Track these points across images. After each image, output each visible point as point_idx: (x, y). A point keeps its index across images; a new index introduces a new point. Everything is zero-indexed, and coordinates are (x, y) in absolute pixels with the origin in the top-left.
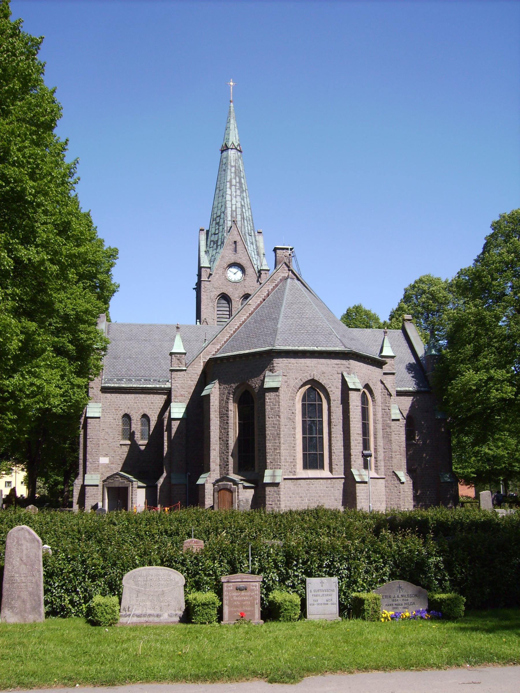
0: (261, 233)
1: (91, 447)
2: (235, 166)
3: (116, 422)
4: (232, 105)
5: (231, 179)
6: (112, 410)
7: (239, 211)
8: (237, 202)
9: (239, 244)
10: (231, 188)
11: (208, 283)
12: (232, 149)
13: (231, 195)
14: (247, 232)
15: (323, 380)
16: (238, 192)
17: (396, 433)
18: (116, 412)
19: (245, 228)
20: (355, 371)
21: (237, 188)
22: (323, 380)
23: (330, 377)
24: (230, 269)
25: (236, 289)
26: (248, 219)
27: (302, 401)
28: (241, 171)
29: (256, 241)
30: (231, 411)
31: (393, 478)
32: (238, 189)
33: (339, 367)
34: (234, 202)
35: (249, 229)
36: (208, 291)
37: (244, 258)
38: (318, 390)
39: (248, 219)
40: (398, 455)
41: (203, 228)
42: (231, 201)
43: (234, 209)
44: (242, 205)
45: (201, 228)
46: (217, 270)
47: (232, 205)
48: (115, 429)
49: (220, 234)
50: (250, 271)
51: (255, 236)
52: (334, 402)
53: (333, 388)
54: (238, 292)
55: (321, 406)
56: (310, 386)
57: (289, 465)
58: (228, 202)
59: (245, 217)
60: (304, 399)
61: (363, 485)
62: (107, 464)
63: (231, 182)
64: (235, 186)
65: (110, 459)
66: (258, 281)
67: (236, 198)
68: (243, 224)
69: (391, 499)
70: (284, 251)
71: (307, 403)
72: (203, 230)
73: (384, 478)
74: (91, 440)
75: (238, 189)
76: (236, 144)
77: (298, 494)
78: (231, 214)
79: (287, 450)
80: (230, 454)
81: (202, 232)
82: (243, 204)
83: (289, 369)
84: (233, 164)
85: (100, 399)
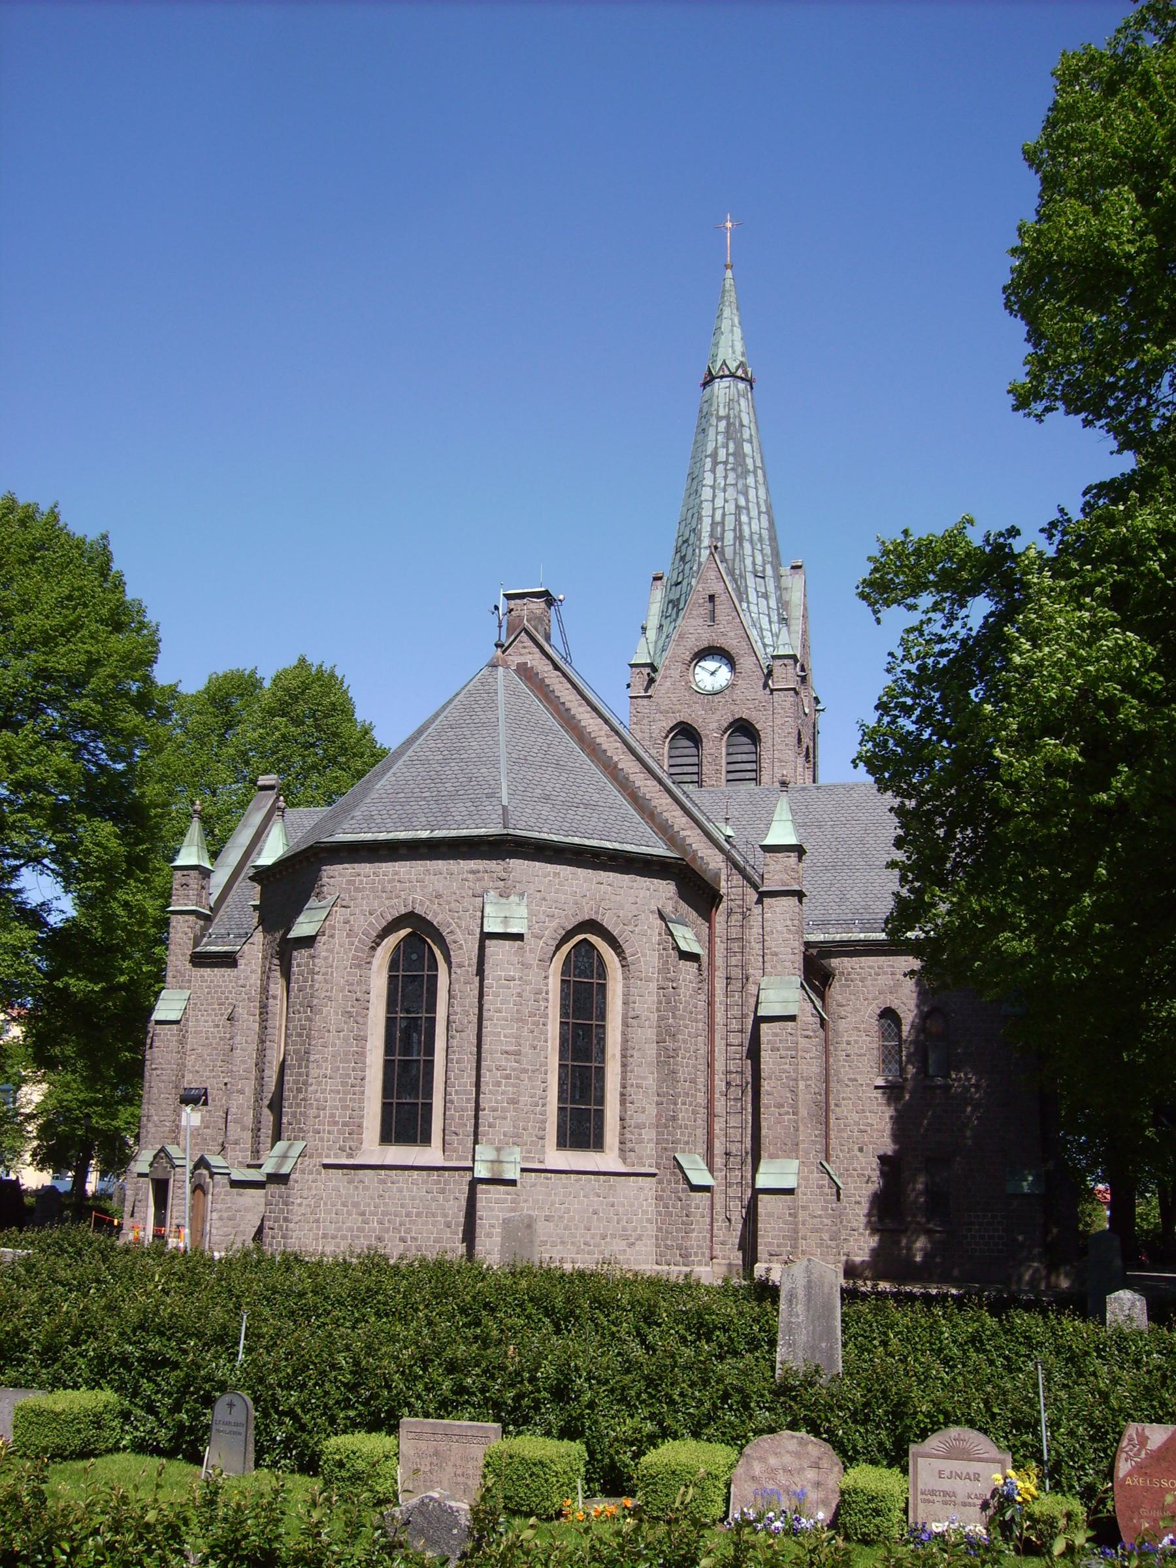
0: (800, 567)
1: (159, 1088)
2: (727, 417)
3: (219, 1032)
4: (729, 273)
5: (716, 448)
6: (212, 1004)
7: (730, 522)
8: (726, 501)
9: (721, 599)
10: (713, 471)
11: (645, 702)
12: (722, 377)
13: (713, 487)
14: (750, 567)
15: (436, 914)
16: (732, 477)
17: (783, 1053)
18: (220, 1009)
19: (743, 560)
20: (532, 888)
21: (729, 467)
22: (436, 914)
23: (453, 905)
24: (702, 664)
25: (713, 710)
26: (756, 537)
27: (563, 974)
28: (742, 425)
29: (778, 587)
30: (275, 997)
31: (674, 1174)
32: (733, 469)
33: (479, 880)
34: (719, 502)
35: (759, 559)
36: (645, 721)
37: (732, 634)
38: (429, 940)
39: (756, 537)
40: (788, 1113)
41: (659, 573)
42: (713, 501)
43: (718, 518)
44: (738, 507)
45: (654, 573)
46: (667, 668)
47: (714, 509)
48: (216, 1049)
49: (685, 583)
50: (746, 663)
51: (778, 577)
52: (459, 971)
53: (459, 936)
54: (716, 717)
55: (434, 980)
56: (409, 930)
57: (340, 1132)
58: (705, 505)
59: (746, 533)
60: (393, 965)
61: (502, 1188)
62: (197, 1129)
63: (714, 455)
64: (726, 463)
65: (202, 1116)
66: (766, 685)
67: (725, 491)
68: (739, 553)
69: (667, 1232)
70: (525, 601)
71: (572, 979)
72: (660, 578)
73: (654, 1175)
74: (159, 1072)
75: (733, 469)
76: (733, 366)
77: (356, 1205)
78: (712, 531)
79: (338, 1092)
80: (266, 1102)
81: (659, 583)
82: (742, 502)
83: (357, 890)
84: (722, 413)
85: (190, 981)
